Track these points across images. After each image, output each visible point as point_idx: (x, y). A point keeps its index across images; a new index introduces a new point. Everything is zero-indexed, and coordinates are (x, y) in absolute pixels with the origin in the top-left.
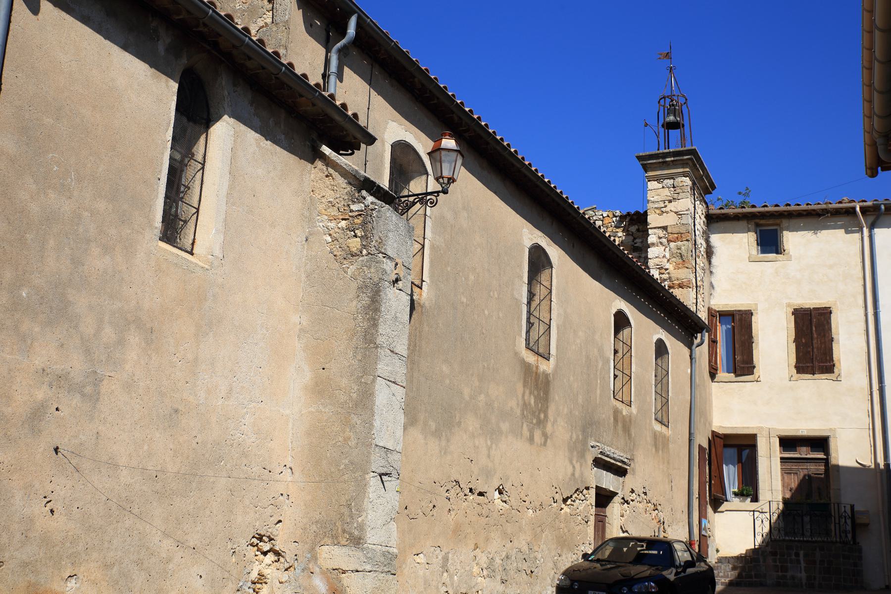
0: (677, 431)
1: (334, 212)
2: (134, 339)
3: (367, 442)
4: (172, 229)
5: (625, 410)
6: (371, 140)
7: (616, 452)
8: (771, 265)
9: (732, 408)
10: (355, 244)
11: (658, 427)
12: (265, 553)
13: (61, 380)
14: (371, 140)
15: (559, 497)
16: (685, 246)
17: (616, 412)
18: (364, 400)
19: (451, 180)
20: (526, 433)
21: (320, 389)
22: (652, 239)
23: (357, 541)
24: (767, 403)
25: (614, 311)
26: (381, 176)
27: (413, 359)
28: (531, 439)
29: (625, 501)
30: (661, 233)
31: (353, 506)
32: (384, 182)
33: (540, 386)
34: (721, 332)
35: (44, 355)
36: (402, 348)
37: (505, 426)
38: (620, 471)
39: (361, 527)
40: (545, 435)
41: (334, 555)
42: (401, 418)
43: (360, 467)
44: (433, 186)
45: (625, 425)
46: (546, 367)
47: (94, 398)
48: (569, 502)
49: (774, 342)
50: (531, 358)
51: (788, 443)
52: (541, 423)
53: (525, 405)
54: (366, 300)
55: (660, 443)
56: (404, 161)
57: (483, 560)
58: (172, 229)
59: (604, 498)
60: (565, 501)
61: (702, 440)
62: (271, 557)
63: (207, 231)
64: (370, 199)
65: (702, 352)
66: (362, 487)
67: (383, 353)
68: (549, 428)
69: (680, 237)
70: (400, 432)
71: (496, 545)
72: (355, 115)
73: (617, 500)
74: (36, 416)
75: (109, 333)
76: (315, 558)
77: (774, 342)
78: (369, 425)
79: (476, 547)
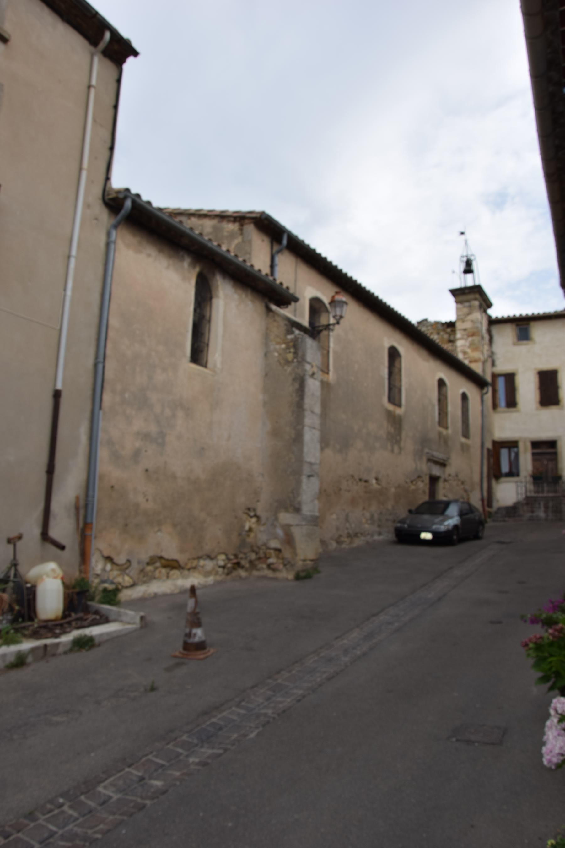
0: (475, 441)
1: (278, 340)
2: (180, 414)
3: (300, 460)
4: (198, 355)
5: (444, 432)
6: (296, 300)
7: (439, 455)
8: (523, 348)
9: (507, 426)
10: (290, 356)
11: (463, 440)
12: (251, 517)
13: (146, 437)
14: (296, 300)
15: (408, 481)
16: (476, 339)
17: (440, 434)
18: (298, 438)
19: (341, 317)
20: (389, 447)
21: (275, 433)
22: (458, 335)
23: (297, 510)
24: (527, 421)
25: (437, 378)
26: (303, 316)
27: (324, 415)
28: (392, 451)
29: (445, 481)
30: (463, 333)
31: (296, 491)
32: (305, 322)
33: (396, 422)
34: (501, 384)
35: (138, 424)
36: (318, 409)
37: (377, 445)
38: (443, 464)
39: (300, 503)
40: (400, 449)
41: (285, 517)
42: (318, 446)
43: (298, 473)
44: (332, 321)
45: (444, 440)
46: (399, 411)
47: (162, 445)
48: (414, 483)
49: (528, 389)
50: (391, 407)
51: (536, 444)
52: (398, 442)
53: (389, 433)
54: (297, 386)
55: (465, 448)
56: (316, 306)
57: (368, 515)
58: (198, 355)
59: (434, 480)
60: (412, 482)
61: (489, 445)
62: (254, 520)
63: (215, 354)
64: (297, 332)
65: (489, 397)
66: (299, 483)
67: (307, 413)
68: (402, 444)
69: (473, 335)
70: (318, 454)
71: (374, 508)
72: (288, 288)
73: (441, 480)
74: (137, 454)
75: (168, 412)
76: (276, 519)
77: (528, 389)
78: (301, 451)
79: (364, 509)
